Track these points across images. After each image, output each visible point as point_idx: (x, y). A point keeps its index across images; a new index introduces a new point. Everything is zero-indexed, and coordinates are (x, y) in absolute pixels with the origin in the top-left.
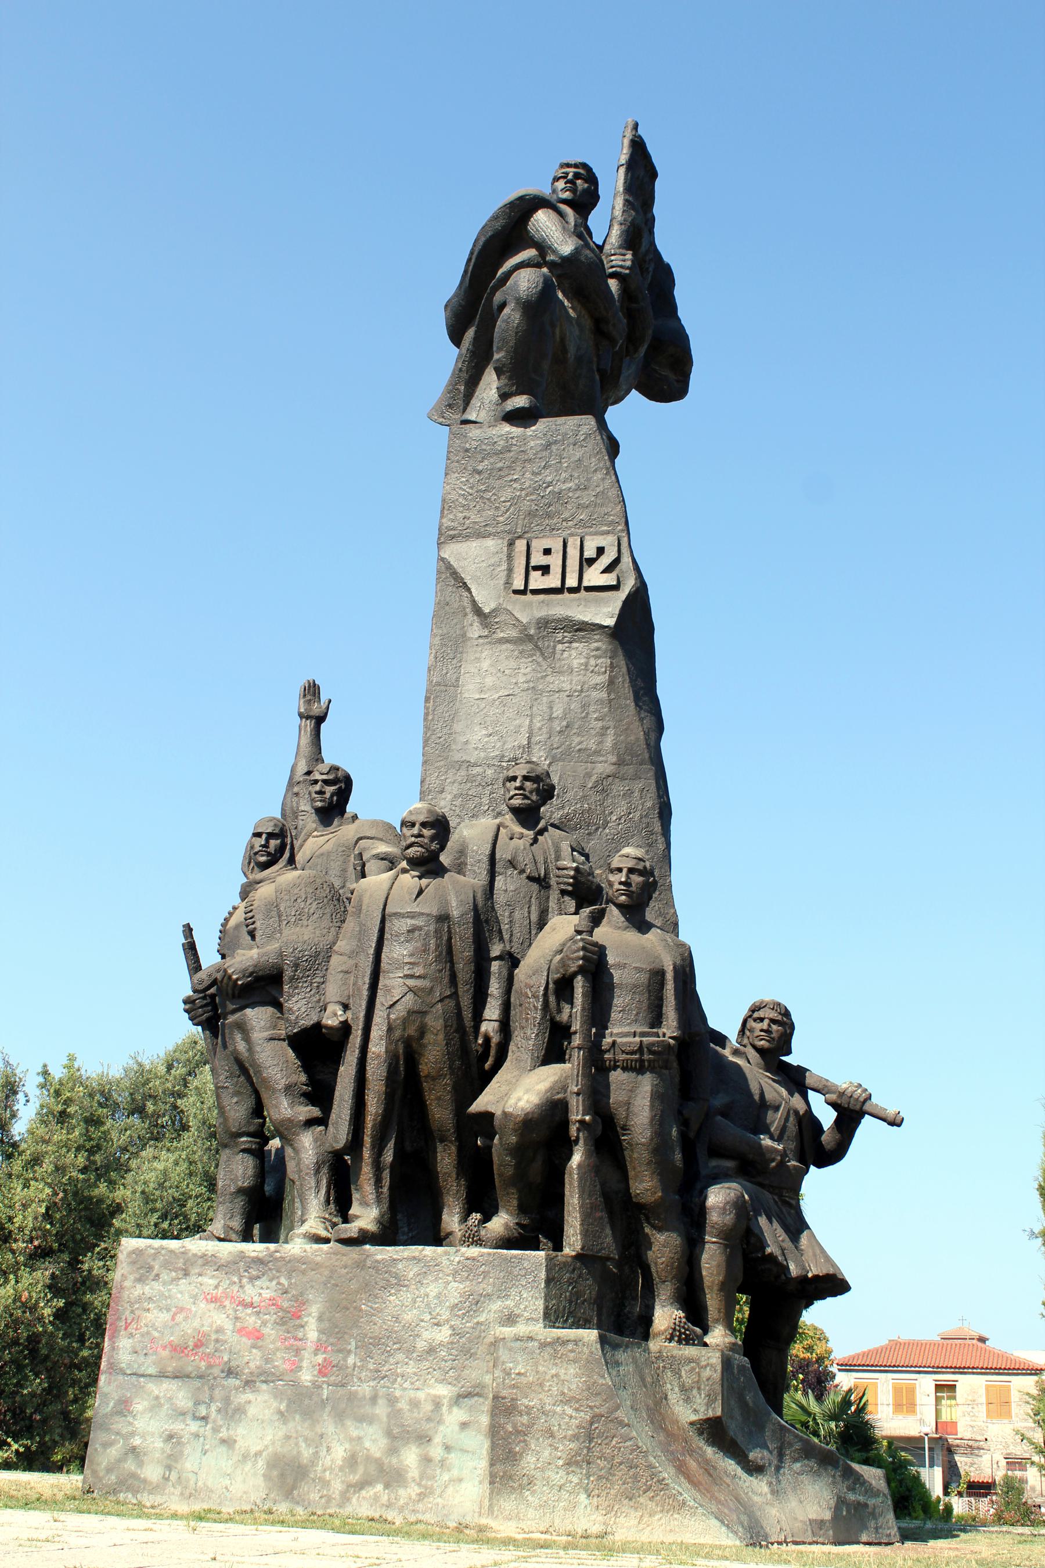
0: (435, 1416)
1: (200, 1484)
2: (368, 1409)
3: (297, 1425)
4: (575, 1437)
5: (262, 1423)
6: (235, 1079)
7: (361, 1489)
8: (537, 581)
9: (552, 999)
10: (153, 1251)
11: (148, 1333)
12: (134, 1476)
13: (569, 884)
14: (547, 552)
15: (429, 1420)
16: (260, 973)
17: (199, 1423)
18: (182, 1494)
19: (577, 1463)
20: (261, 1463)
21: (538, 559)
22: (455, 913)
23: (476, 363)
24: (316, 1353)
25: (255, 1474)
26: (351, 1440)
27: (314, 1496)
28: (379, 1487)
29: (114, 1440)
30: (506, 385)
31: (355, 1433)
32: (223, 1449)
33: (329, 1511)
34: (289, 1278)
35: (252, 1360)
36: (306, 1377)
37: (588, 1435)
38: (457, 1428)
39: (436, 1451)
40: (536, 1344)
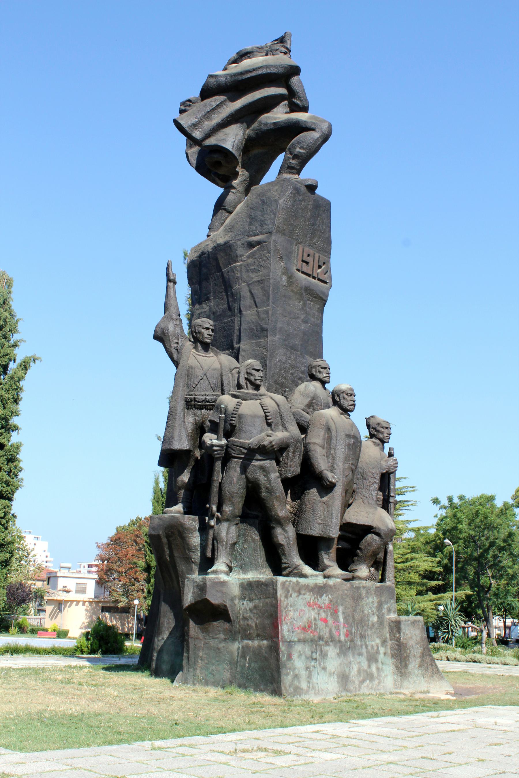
7: (363, 682)
8: (305, 268)
18: (315, 693)
20: (335, 676)
23: (230, 120)
30: (296, 164)
31: (358, 660)
34: (332, 595)
35: (325, 633)
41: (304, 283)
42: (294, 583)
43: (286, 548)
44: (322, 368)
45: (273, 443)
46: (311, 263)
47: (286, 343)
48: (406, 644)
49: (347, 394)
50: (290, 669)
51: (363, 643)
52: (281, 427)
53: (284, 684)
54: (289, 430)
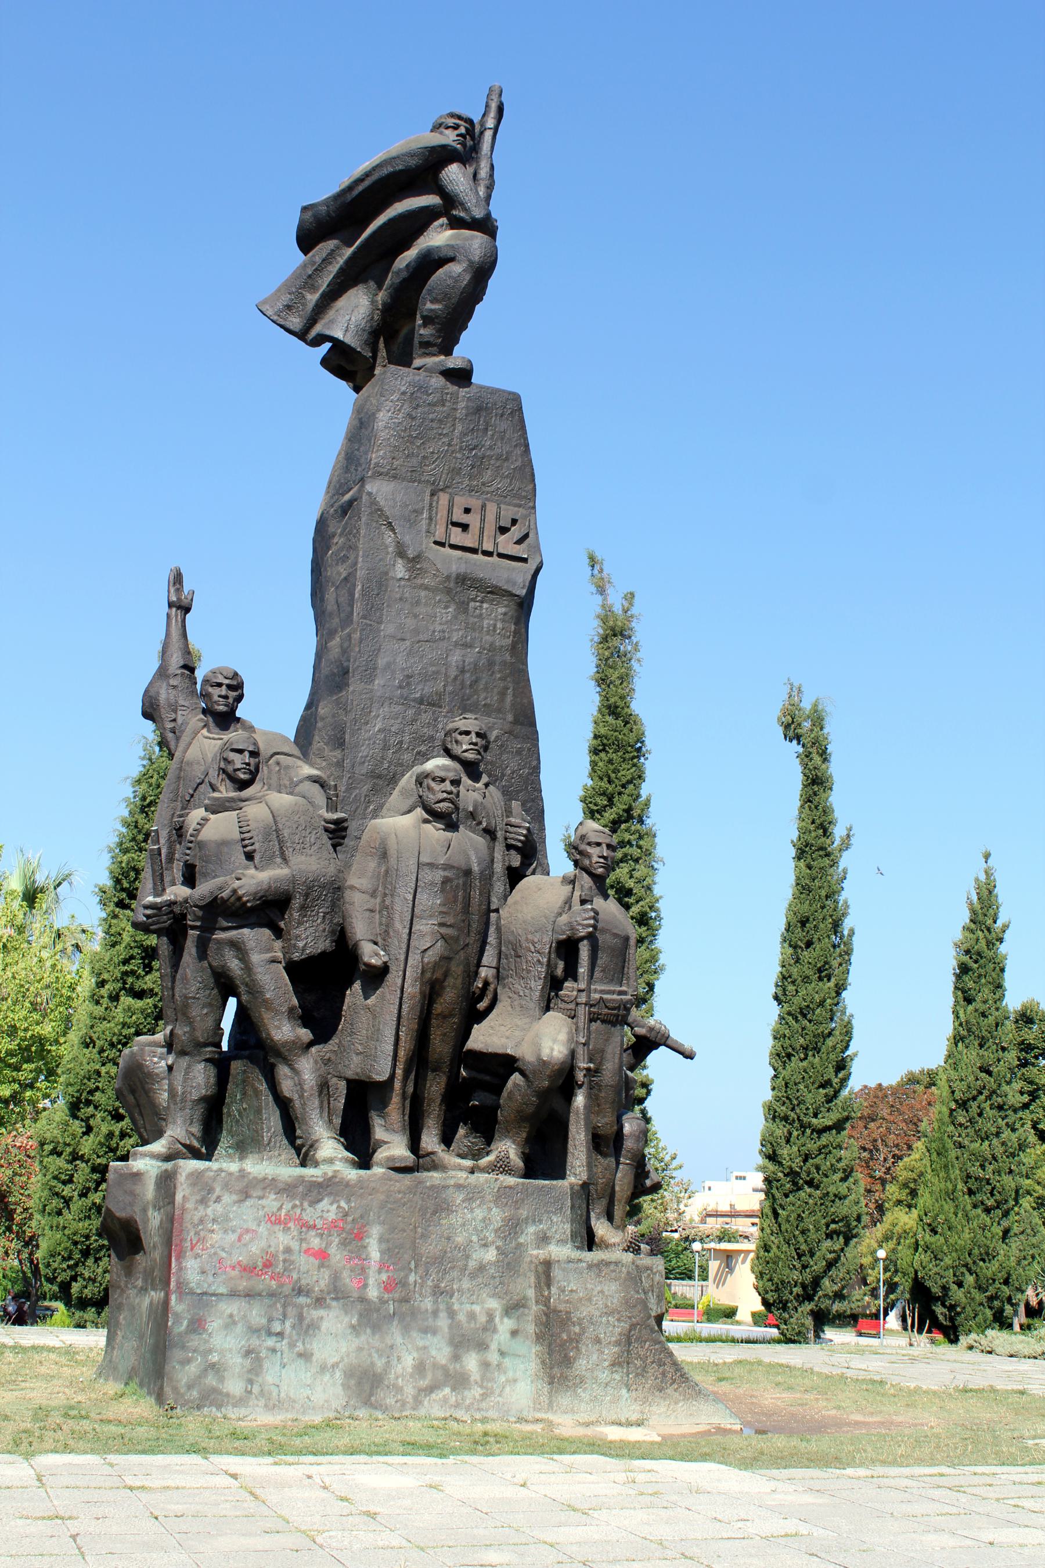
0: (490, 1326)
1: (282, 1395)
2: (430, 1322)
3: (366, 1338)
4: (618, 1343)
5: (336, 1336)
6: (208, 992)
7: (431, 1392)
8: (457, 536)
9: (553, 956)
10: (212, 1174)
11: (215, 1254)
12: (215, 1390)
13: (520, 841)
14: (467, 511)
15: (485, 1329)
16: (270, 898)
17: (274, 1338)
18: (266, 1406)
19: (620, 1364)
20: (338, 1374)
21: (459, 516)
22: (476, 868)
24: (380, 1272)
25: (334, 1384)
26: (418, 1349)
27: (390, 1401)
28: (447, 1390)
29: (192, 1357)
31: (421, 1343)
32: (301, 1362)
33: (404, 1414)
34: (348, 1202)
35: (320, 1280)
36: (373, 1293)
37: (627, 1340)
38: (508, 1335)
39: (493, 1357)
40: (584, 1265)
41: (455, 569)
42: (231, 1174)
43: (297, 1104)
44: (461, 734)
45: (240, 892)
46: (475, 527)
47: (405, 692)
48: (568, 1313)
49: (434, 779)
50: (194, 1351)
51: (442, 1307)
52: (279, 860)
53: (171, 1379)
54: (291, 863)
